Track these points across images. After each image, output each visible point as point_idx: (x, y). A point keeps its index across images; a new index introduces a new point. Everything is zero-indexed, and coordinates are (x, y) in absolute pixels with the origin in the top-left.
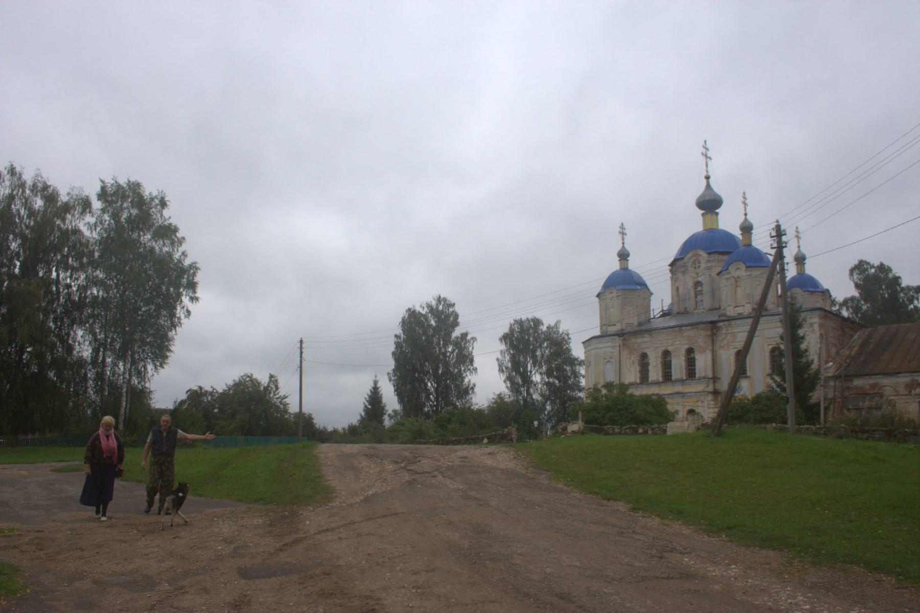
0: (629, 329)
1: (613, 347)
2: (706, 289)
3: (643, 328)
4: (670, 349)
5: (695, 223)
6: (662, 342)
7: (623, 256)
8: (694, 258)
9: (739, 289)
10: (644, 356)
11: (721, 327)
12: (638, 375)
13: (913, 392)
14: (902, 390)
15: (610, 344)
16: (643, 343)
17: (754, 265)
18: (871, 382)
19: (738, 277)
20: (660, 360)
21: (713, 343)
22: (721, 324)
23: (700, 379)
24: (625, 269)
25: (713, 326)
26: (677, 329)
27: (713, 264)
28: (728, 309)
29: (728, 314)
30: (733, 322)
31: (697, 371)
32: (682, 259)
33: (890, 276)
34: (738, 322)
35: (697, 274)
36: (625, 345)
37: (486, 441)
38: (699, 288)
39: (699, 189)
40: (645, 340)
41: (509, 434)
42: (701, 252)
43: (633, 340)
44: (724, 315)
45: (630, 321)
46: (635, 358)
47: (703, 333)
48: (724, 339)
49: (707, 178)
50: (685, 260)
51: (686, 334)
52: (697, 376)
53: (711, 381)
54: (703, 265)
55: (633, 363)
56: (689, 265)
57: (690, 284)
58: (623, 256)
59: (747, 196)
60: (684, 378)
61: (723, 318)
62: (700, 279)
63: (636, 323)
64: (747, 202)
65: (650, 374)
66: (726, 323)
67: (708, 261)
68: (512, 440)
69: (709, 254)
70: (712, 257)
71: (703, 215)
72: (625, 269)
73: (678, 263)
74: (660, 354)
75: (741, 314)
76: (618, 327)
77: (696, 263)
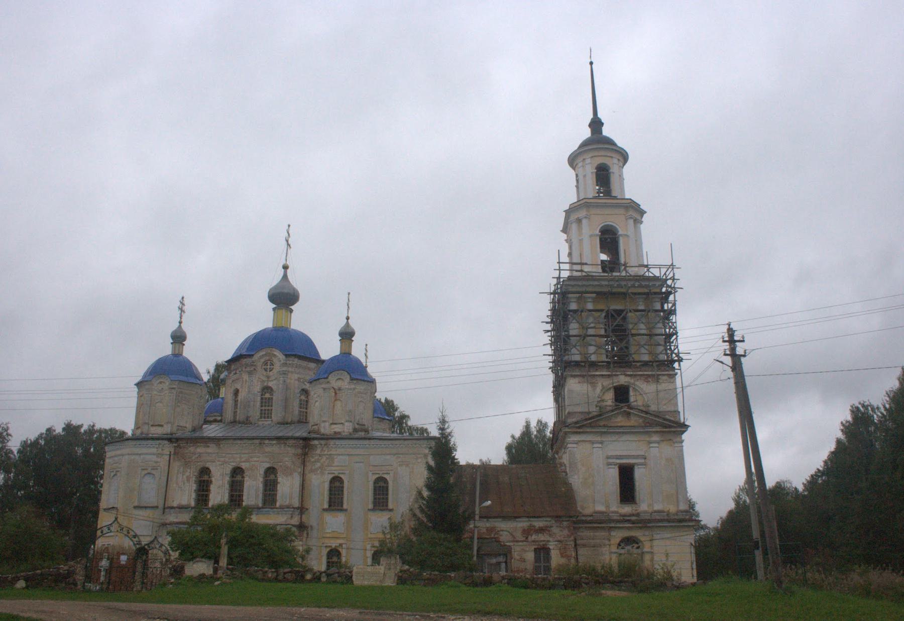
0: (179, 434)
1: (159, 455)
2: (277, 397)
3: (197, 434)
4: (244, 466)
5: (263, 317)
6: (237, 455)
7: (179, 338)
8: (267, 358)
9: (338, 404)
10: (205, 471)
11: (316, 446)
12: (194, 495)
13: (530, 539)
14: (519, 536)
15: (154, 450)
16: (207, 455)
17: (360, 378)
18: (488, 525)
19: (340, 389)
20: (227, 478)
21: (304, 463)
22: (316, 442)
23: (282, 507)
24: (177, 355)
25: (306, 444)
26: (257, 441)
27: (290, 369)
28: (323, 425)
29: (322, 431)
30: (332, 442)
31: (278, 498)
32: (251, 356)
33: (397, 414)
34: (338, 442)
35: (268, 377)
36: (176, 454)
37: (21, 584)
38: (267, 395)
39: (274, 279)
40: (209, 450)
41: (70, 573)
42: (277, 353)
43: (192, 449)
44: (318, 432)
45: (182, 424)
46: (192, 473)
47: (291, 451)
48: (318, 461)
49: (285, 267)
50: (256, 357)
51: (268, 449)
52: (278, 505)
53: (297, 512)
54: (277, 367)
55: (188, 479)
56: (259, 364)
57: (257, 388)
58: (179, 338)
59: (186, 302)
60: (260, 505)
61: (315, 436)
62: (270, 384)
63: (189, 426)
64: (185, 308)
65: (211, 496)
66: (323, 442)
67: (285, 364)
68: (75, 584)
69: (286, 356)
70: (291, 361)
71: (274, 309)
72: (177, 355)
73: (244, 361)
74: (228, 469)
75: (339, 433)
76: (167, 429)
77: (268, 364)
